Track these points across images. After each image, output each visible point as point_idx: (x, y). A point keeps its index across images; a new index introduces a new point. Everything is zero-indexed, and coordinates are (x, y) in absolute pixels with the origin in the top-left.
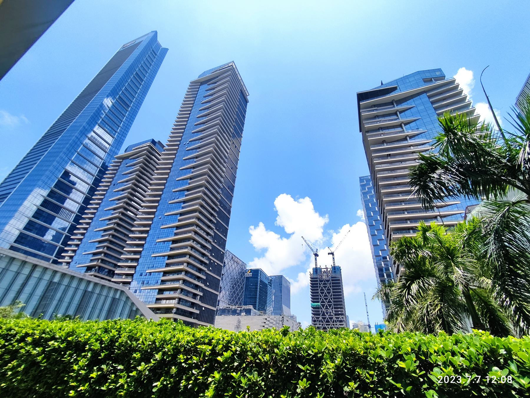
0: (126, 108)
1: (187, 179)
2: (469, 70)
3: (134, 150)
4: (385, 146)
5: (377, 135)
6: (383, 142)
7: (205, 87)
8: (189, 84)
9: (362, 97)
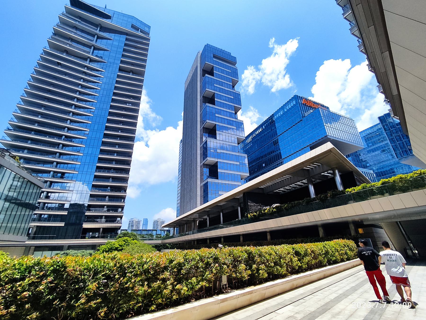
2: (244, 72)
4: (64, 56)
5: (64, 43)
6: (67, 52)
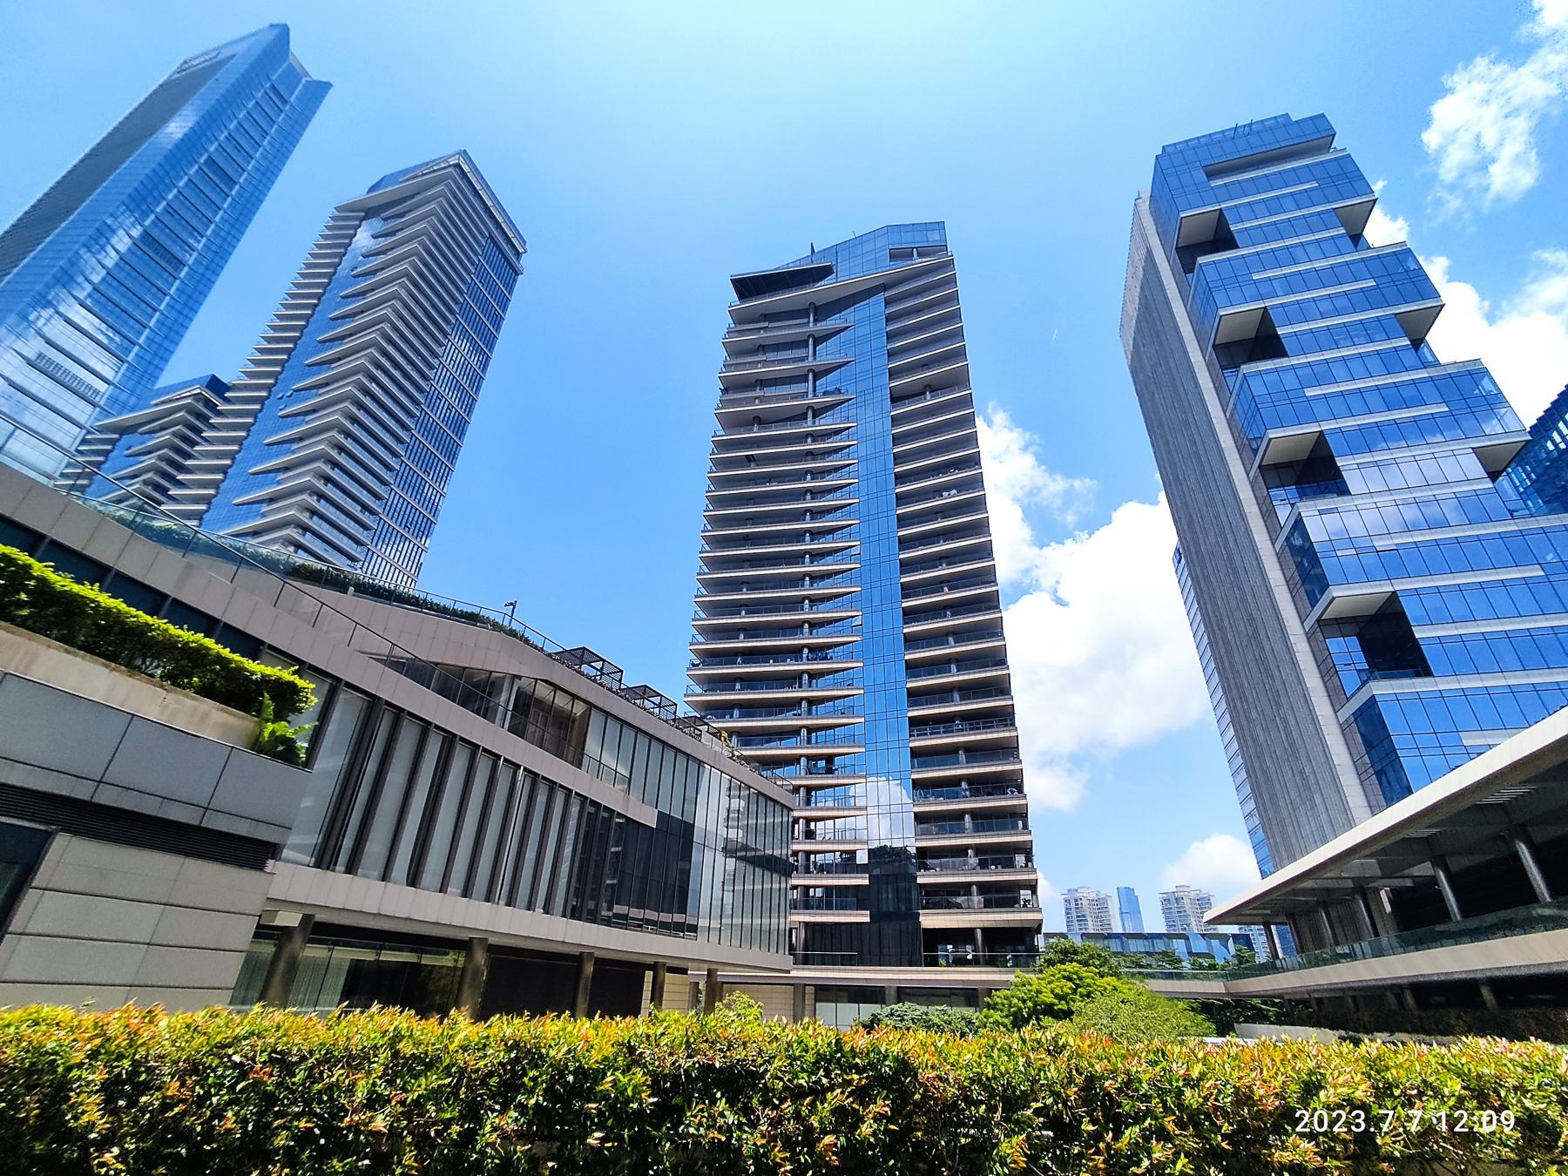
0: (170, 269)
1: (261, 502)
3: (156, 405)
7: (376, 224)
8: (333, 212)
9: (747, 287)
